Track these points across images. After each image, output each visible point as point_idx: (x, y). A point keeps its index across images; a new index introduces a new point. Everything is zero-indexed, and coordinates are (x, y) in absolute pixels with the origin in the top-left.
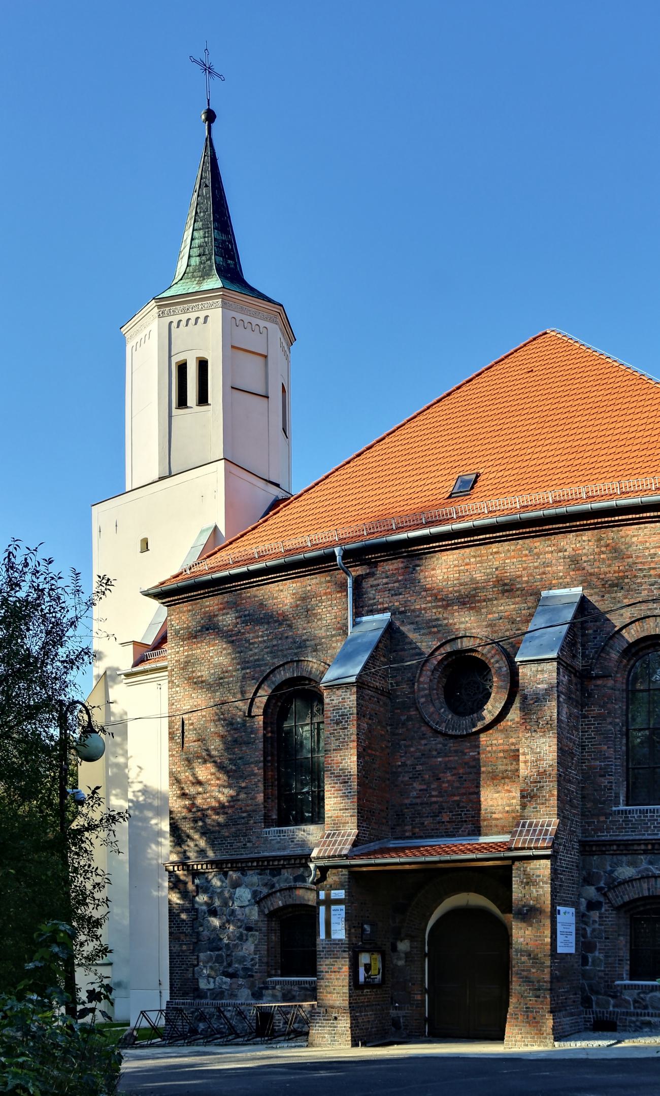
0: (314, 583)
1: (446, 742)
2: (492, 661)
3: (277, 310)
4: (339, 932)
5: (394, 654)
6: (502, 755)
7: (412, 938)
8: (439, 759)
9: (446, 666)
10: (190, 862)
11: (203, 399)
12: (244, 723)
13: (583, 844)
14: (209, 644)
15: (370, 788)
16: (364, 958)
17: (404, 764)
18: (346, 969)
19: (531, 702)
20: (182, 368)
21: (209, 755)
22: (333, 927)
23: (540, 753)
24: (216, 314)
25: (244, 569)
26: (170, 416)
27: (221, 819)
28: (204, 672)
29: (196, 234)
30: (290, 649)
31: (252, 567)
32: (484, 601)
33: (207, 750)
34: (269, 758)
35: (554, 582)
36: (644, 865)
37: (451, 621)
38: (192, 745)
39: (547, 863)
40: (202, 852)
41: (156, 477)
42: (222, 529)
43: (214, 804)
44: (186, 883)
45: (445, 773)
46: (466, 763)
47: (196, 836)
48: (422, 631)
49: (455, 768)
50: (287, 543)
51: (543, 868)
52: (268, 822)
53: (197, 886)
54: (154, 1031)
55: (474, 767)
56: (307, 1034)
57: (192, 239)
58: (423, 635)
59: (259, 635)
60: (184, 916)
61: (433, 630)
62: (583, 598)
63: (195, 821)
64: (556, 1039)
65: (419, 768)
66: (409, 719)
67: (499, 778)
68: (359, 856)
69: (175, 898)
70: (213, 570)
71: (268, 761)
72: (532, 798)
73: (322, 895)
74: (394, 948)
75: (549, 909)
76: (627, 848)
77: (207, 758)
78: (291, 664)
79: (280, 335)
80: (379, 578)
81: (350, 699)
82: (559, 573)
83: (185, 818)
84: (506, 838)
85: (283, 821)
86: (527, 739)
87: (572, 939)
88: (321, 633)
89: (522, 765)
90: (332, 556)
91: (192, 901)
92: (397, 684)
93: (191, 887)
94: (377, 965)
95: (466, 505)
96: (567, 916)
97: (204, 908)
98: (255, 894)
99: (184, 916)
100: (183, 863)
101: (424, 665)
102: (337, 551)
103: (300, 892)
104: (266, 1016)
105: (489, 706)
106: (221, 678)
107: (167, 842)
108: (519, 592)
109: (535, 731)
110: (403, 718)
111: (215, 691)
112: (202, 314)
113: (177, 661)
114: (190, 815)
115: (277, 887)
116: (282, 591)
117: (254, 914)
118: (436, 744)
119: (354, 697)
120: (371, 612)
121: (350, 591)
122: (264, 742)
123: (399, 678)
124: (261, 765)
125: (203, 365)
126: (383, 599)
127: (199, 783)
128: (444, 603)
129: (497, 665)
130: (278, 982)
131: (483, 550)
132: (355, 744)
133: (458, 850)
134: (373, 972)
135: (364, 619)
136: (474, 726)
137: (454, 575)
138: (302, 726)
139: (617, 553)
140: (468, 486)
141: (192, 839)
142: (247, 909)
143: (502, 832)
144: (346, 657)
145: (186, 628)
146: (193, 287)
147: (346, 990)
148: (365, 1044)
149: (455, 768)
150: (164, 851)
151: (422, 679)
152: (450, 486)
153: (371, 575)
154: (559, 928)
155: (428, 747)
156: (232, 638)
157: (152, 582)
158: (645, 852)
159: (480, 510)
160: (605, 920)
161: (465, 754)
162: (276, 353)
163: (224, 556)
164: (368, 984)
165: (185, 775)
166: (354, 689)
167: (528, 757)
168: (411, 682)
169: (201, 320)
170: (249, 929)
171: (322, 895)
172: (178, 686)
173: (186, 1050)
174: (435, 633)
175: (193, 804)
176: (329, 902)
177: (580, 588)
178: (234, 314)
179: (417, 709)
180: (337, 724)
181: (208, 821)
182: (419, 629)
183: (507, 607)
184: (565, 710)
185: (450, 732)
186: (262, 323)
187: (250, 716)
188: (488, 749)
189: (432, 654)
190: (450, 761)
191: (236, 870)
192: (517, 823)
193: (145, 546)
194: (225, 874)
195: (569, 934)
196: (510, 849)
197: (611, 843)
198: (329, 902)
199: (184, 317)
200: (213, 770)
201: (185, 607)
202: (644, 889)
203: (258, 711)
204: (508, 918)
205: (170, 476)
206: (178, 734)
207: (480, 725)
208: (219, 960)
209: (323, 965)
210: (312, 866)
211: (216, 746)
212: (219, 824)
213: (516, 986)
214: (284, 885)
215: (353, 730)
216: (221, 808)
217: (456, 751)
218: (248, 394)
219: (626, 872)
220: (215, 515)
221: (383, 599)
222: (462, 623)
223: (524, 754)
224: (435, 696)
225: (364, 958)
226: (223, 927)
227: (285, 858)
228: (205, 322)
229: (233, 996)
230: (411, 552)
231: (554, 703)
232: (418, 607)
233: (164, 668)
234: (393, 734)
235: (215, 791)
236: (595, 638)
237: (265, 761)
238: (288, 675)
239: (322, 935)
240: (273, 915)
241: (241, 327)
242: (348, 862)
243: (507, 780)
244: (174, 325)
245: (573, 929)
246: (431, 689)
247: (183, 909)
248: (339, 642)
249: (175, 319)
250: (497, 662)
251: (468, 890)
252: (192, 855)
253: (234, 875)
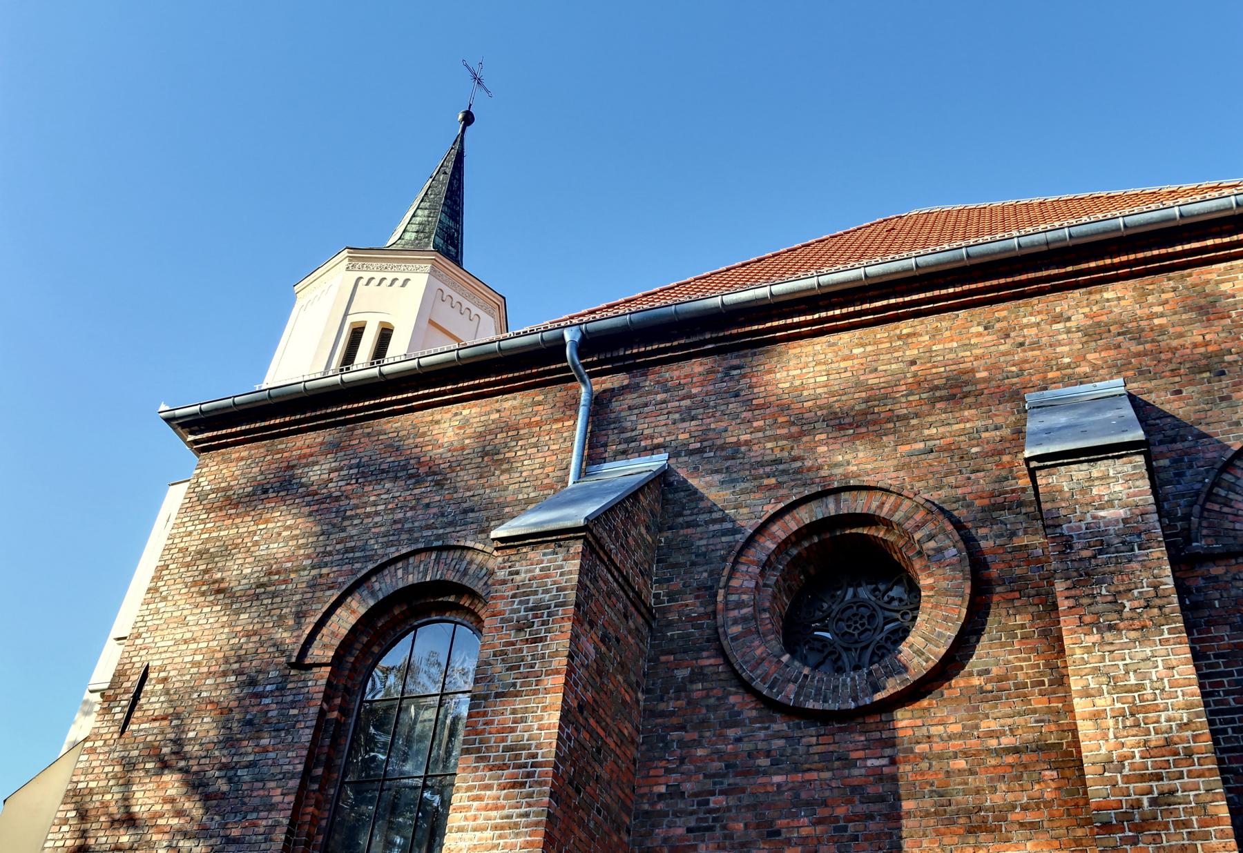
1: (797, 733)
2: (917, 536)
5: (669, 534)
6: (961, 764)
8: (777, 779)
9: (795, 562)
15: (582, 824)
17: (675, 793)
19: (1086, 553)
20: (357, 334)
23: (1140, 687)
24: (419, 279)
29: (420, 212)
30: (428, 527)
32: (889, 421)
34: (319, 771)
35: (1050, 375)
37: (808, 463)
45: (795, 816)
46: (854, 789)
48: (741, 486)
49: (824, 803)
55: (881, 799)
57: (414, 216)
58: (742, 492)
61: (766, 482)
65: (716, 801)
66: (698, 675)
71: (314, 779)
72: (1139, 829)
78: (423, 556)
80: (649, 393)
81: (563, 568)
86: (1089, 650)
90: (559, 344)
92: (672, 597)
101: (741, 553)
102: (568, 335)
106: (262, 585)
108: (968, 400)
109: (1111, 628)
110: (682, 673)
112: (402, 277)
113: (180, 550)
116: (437, 422)
118: (767, 739)
119: (574, 565)
122: (317, 729)
123: (677, 584)
124: (294, 783)
128: (794, 429)
129: (932, 544)
132: (561, 679)
136: (876, 689)
139: (1208, 308)
145: (225, 490)
149: (824, 803)
151: (735, 583)
155: (746, 746)
161: (852, 764)
166: (578, 546)
167: (1102, 702)
168: (707, 592)
172: (165, 599)
174: (769, 488)
177: (1120, 381)
179: (721, 652)
180: (520, 629)
182: (733, 481)
185: (810, 705)
186: (475, 310)
188: (918, 749)
189: (762, 529)
190: (810, 782)
203: (322, 652)
207: (893, 686)
215: (559, 642)
217: (826, 757)
221: (649, 426)
222: (837, 465)
223: (1086, 693)
228: (403, 285)
232: (734, 439)
234: (652, 713)
236: (1180, 475)
237: (306, 776)
238: (412, 579)
243: (983, 836)
246: (758, 609)
249: (366, 276)
250: (931, 537)
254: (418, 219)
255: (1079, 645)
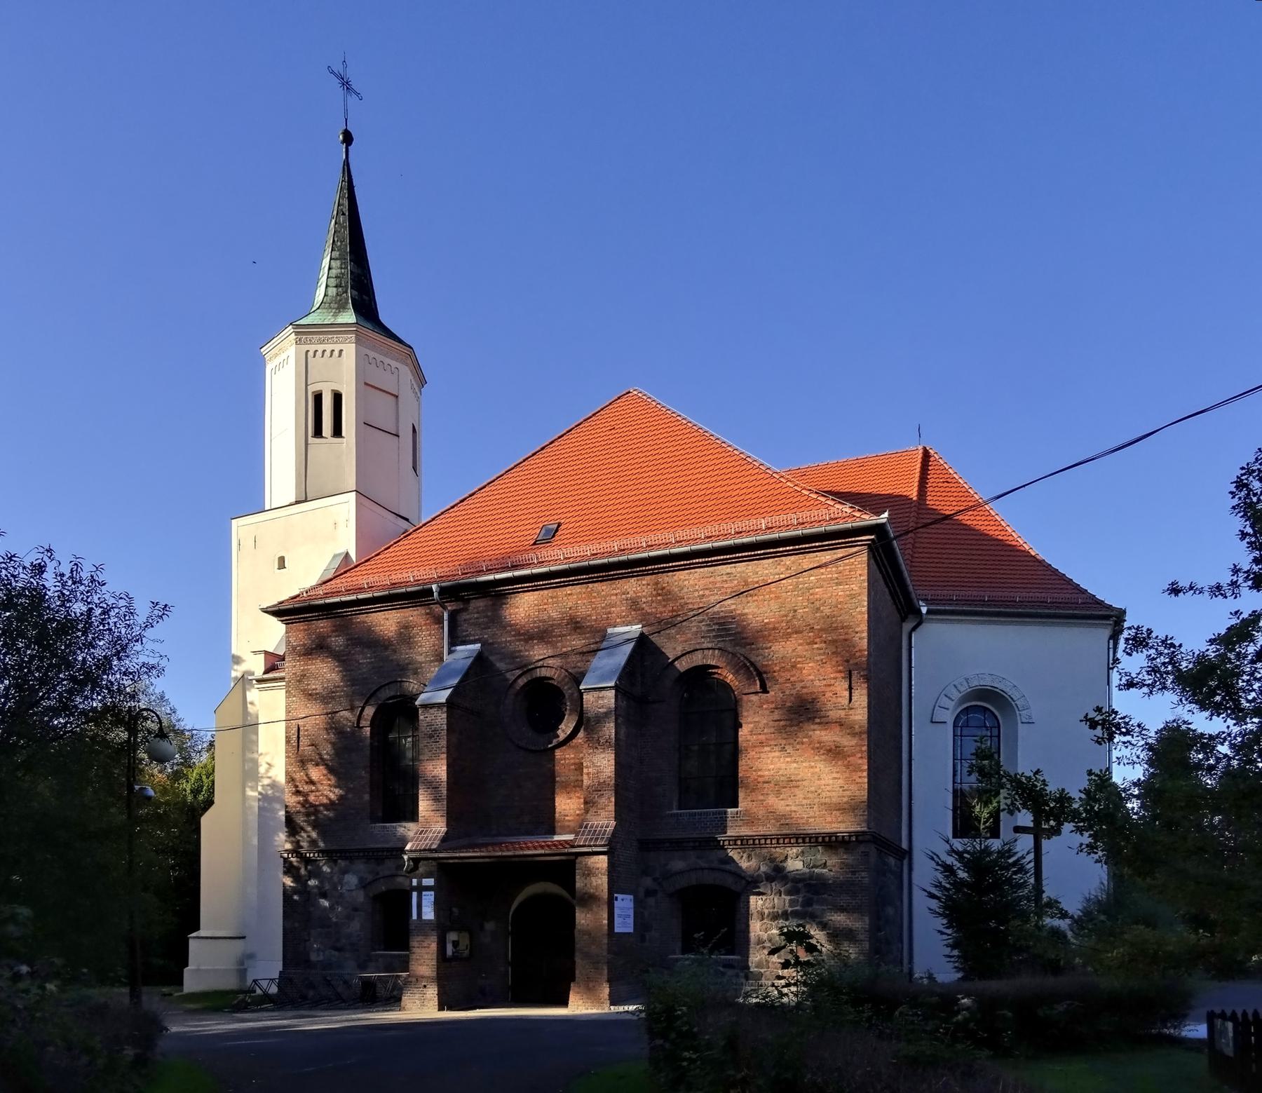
0: (414, 615)
4: (429, 914)
10: (303, 851)
11: (337, 432)
12: (353, 733)
14: (323, 661)
16: (452, 936)
18: (434, 946)
20: (318, 398)
21: (322, 759)
22: (425, 909)
24: (350, 349)
25: (353, 597)
26: (307, 444)
27: (331, 814)
28: (315, 686)
31: (361, 596)
33: (320, 754)
38: (306, 749)
39: (604, 858)
40: (313, 842)
41: (293, 500)
42: (353, 555)
43: (325, 801)
44: (298, 869)
47: (309, 829)
50: (393, 577)
51: (602, 862)
52: (374, 819)
53: (309, 872)
54: (267, 997)
56: (400, 1000)
59: (364, 659)
60: (296, 897)
63: (308, 815)
64: (612, 1004)
67: (599, 788)
68: (446, 850)
69: (288, 881)
70: (326, 595)
73: (415, 882)
74: (482, 928)
75: (605, 895)
77: (321, 761)
79: (410, 377)
81: (441, 718)
82: (621, 614)
83: (299, 812)
84: (570, 837)
87: (631, 921)
88: (420, 658)
89: (585, 777)
91: (305, 884)
93: (303, 871)
94: (465, 941)
95: (546, 553)
96: (624, 904)
97: (316, 890)
98: (361, 880)
99: (296, 897)
100: (296, 851)
102: (434, 587)
103: (400, 879)
104: (368, 985)
105: (562, 726)
107: (282, 836)
111: (327, 703)
112: (337, 348)
114: (302, 810)
115: (381, 874)
117: (360, 897)
120: (464, 643)
121: (446, 623)
125: (337, 398)
126: (473, 631)
127: (312, 782)
130: (381, 956)
131: (560, 592)
133: (533, 847)
134: (462, 947)
135: (459, 648)
137: (533, 613)
138: (406, 738)
140: (550, 536)
141: (306, 832)
142: (354, 893)
143: (570, 833)
144: (438, 683)
146: (329, 320)
147: (434, 962)
148: (451, 1008)
150: (282, 841)
152: (535, 533)
153: (465, 610)
154: (617, 912)
156: (342, 659)
157: (271, 601)
159: (557, 557)
163: (339, 584)
164: (455, 958)
165: (300, 776)
169: (336, 353)
170: (356, 909)
171: (415, 882)
173: (291, 1013)
175: (306, 801)
178: (368, 352)
181: (320, 816)
183: (577, 642)
186: (394, 364)
187: (358, 726)
191: (346, 858)
192: (580, 826)
193: (282, 563)
194: (335, 862)
196: (573, 847)
198: (421, 889)
199: (320, 348)
200: (325, 772)
201: (301, 626)
203: (365, 723)
204: (575, 902)
205: (306, 501)
206: (294, 740)
207: (555, 742)
209: (414, 942)
210: (406, 857)
211: (327, 751)
212: (330, 819)
213: (578, 960)
214: (387, 873)
215: (444, 743)
216: (331, 805)
218: (378, 433)
220: (347, 543)
221: (473, 631)
224: (513, 715)
225: (452, 936)
226: (332, 907)
227: (388, 850)
230: (495, 593)
231: (612, 725)
233: (282, 679)
235: (326, 790)
240: (378, 898)
241: (374, 366)
242: (436, 855)
244: (311, 354)
245: (631, 913)
247: (294, 891)
248: (436, 667)
249: (312, 348)
251: (546, 880)
252: (304, 844)
253: (342, 863)
254: (334, 272)
255: (671, 657)
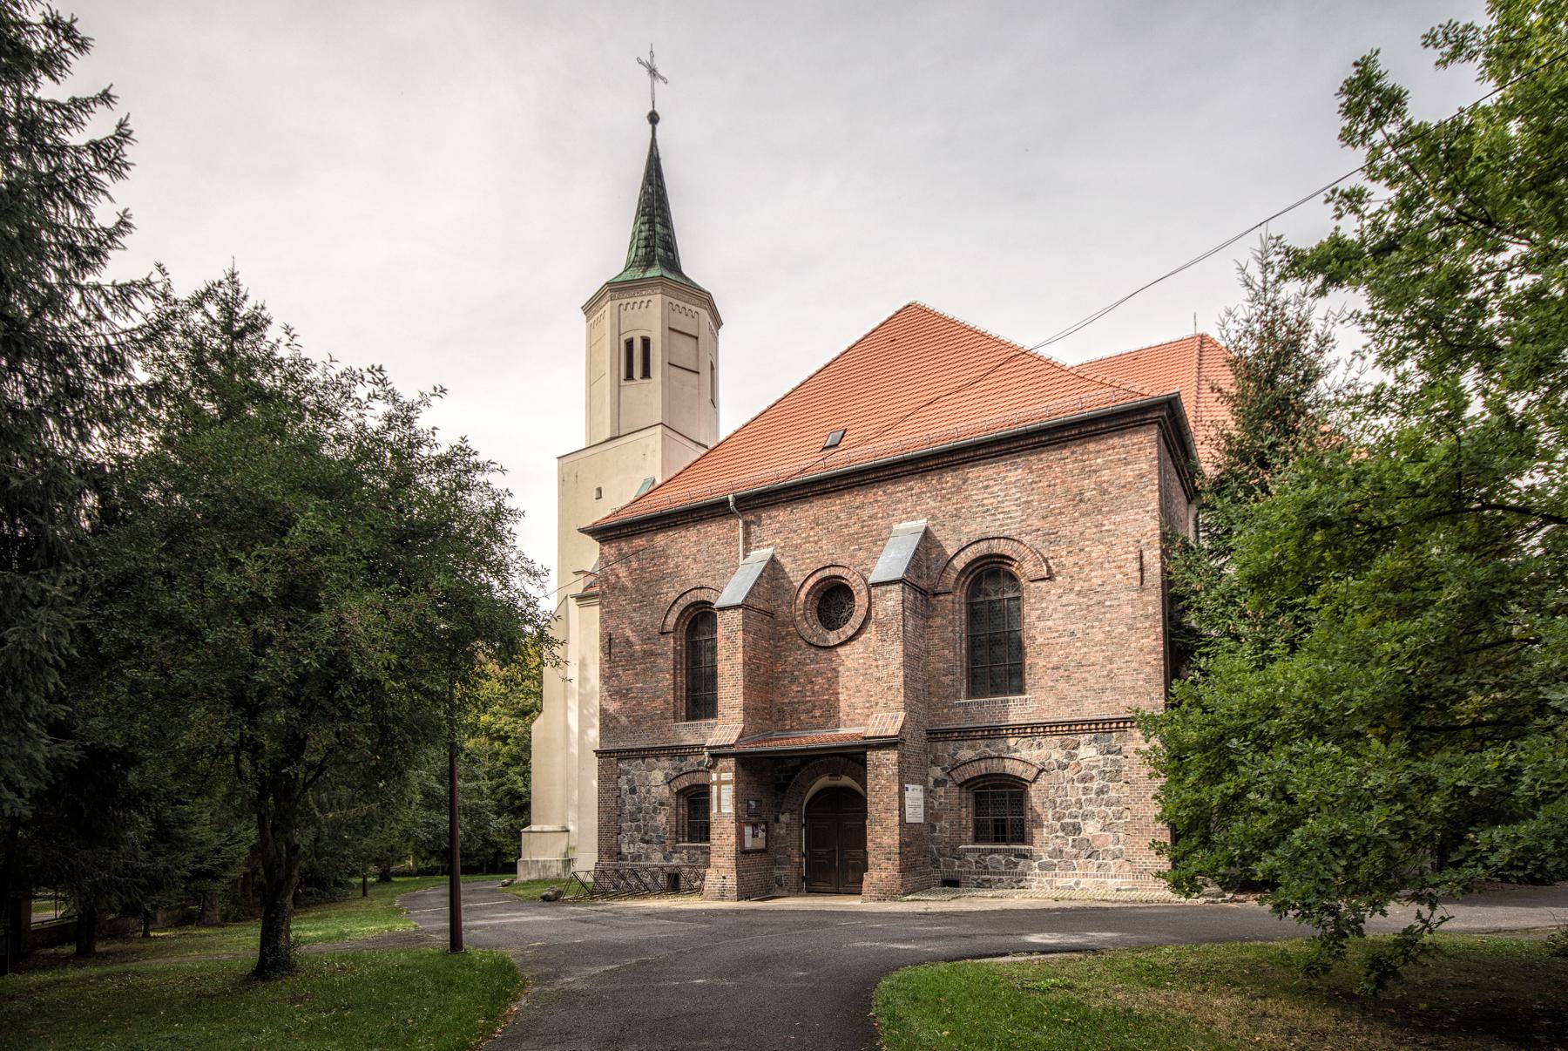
3: (705, 299)
7: (792, 812)
11: (646, 374)
13: (929, 732)
17: (784, 671)
20: (630, 344)
36: (983, 748)
62: (927, 530)
74: (777, 820)
76: (965, 734)
81: (737, 616)
85: (692, 716)
87: (921, 811)
90: (727, 501)
102: (730, 497)
112: (646, 299)
117: (665, 792)
154: (908, 802)
157: (588, 523)
158: (982, 737)
160: (949, 795)
162: (704, 335)
170: (662, 804)
176: (720, 783)
184: (911, 623)
186: (694, 309)
195: (915, 807)
197: (952, 731)
198: (720, 783)
202: (983, 768)
208: (638, 829)
214: (689, 769)
219: (966, 754)
229: (648, 858)
239: (714, 810)
245: (921, 803)
